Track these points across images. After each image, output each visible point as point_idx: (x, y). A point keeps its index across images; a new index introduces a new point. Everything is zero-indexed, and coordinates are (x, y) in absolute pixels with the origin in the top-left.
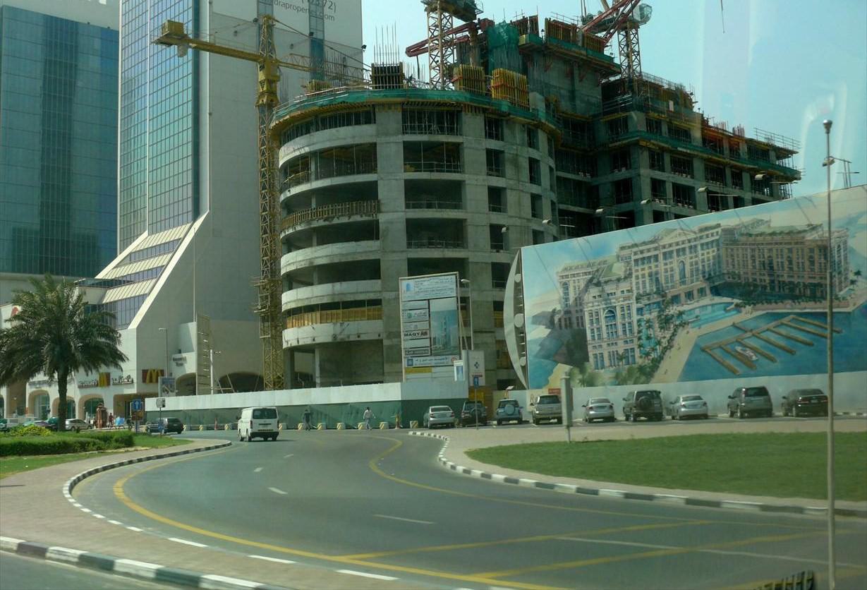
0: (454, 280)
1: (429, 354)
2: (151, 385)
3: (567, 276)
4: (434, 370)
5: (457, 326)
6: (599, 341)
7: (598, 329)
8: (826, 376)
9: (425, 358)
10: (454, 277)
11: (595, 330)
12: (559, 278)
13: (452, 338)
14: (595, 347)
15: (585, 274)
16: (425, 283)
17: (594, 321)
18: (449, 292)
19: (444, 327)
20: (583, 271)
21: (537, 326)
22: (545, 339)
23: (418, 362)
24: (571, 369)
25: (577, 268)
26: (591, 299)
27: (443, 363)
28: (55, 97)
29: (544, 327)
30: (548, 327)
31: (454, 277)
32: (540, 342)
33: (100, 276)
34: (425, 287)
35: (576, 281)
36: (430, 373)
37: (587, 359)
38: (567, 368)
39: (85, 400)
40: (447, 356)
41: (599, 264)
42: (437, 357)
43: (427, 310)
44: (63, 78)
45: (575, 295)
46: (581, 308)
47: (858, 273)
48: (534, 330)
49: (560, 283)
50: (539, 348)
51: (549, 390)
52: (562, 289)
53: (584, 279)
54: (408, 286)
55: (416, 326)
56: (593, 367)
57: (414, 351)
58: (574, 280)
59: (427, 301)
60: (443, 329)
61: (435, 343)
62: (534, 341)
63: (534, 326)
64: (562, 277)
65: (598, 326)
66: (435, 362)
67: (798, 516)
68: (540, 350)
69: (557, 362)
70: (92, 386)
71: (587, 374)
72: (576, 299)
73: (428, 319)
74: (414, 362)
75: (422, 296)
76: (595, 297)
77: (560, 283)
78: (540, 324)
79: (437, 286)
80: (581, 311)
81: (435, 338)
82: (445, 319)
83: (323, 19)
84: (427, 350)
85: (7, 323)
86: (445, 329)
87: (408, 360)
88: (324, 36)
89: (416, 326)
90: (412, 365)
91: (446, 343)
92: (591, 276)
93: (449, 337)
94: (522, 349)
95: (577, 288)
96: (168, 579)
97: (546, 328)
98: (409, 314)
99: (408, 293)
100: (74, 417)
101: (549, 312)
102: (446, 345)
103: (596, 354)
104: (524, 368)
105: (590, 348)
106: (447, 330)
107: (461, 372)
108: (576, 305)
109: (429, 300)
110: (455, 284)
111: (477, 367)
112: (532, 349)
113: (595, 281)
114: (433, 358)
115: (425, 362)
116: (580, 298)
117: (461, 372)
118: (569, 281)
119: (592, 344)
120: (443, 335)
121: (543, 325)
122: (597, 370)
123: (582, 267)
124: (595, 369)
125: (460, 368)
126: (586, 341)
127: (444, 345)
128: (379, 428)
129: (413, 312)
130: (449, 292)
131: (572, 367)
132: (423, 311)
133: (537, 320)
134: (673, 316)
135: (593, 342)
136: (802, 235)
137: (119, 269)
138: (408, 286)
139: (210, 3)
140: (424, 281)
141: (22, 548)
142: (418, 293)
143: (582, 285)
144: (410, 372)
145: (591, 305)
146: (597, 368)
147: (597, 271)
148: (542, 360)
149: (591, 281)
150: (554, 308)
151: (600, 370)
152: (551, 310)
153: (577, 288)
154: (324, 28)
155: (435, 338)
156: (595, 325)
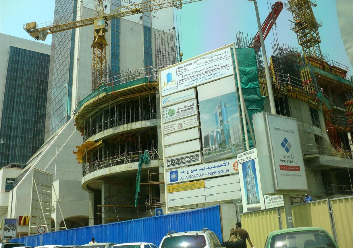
0: (229, 54)
2: (25, 227)
4: (207, 183)
5: (238, 114)
13: (231, 132)
18: (223, 71)
19: (220, 119)
27: (222, 172)
28: (32, 87)
34: (190, 72)
40: (227, 161)
42: (212, 165)
43: (195, 101)
54: (169, 76)
57: (178, 160)
61: (207, 144)
73: (196, 112)
74: (180, 175)
75: (187, 84)
79: (206, 67)
81: (207, 138)
82: (220, 107)
83: (151, 17)
84: (197, 155)
85: (54, 202)
86: (221, 121)
87: (171, 173)
88: (151, 26)
90: (177, 180)
91: (224, 141)
93: (228, 130)
96: (289, 168)
102: (223, 144)
106: (225, 122)
107: (250, 172)
109: (196, 88)
110: (230, 58)
111: (287, 150)
114: (206, 166)
115: (194, 173)
117: (250, 172)
125: (250, 165)
127: (220, 145)
129: (175, 108)
130: (223, 71)
132: (189, 103)
139: (81, 2)
142: (181, 82)
144: (177, 190)
154: (151, 22)
155: (207, 138)
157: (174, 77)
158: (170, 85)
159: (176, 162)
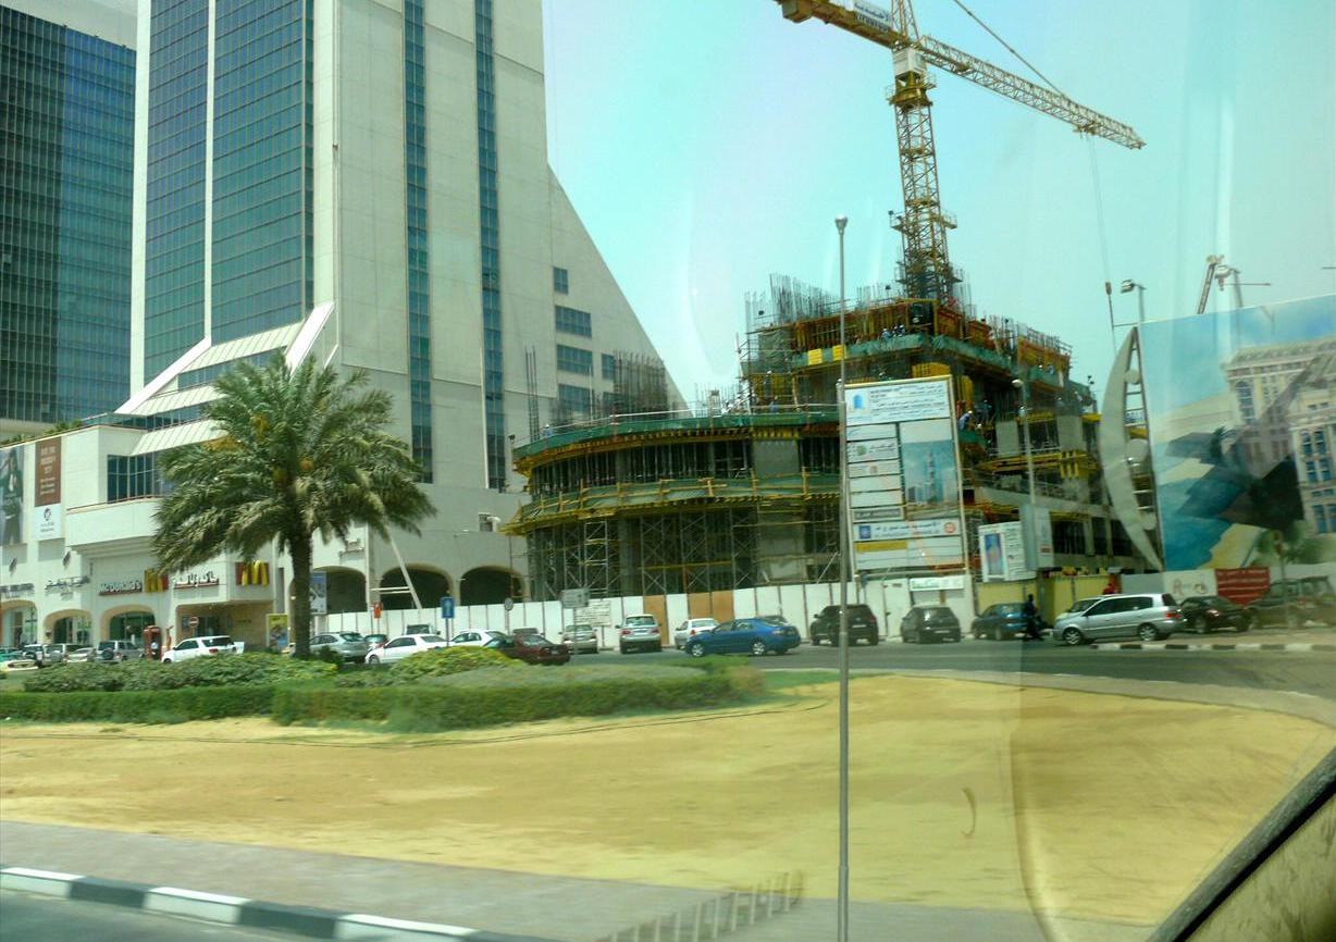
1: (901, 518)
3: (1245, 372)
4: (911, 544)
9: (894, 525)
10: (945, 382)
11: (1317, 464)
12: (1227, 374)
14: (1317, 494)
15: (1289, 366)
16: (890, 395)
17: (1314, 447)
19: (930, 470)
20: (1285, 362)
21: (1181, 459)
22: (1200, 482)
23: (881, 532)
24: (1263, 535)
26: (1305, 409)
27: (930, 532)
29: (1198, 460)
32: (1189, 486)
33: (125, 410)
36: (904, 551)
37: (1299, 513)
38: (1253, 532)
40: (937, 521)
41: (1320, 349)
44: (16, 103)
49: (1232, 382)
50: (1185, 498)
53: (1287, 376)
54: (857, 400)
57: (872, 512)
58: (1264, 378)
59: (893, 426)
61: (912, 499)
62: (1176, 487)
63: (1174, 460)
64: (1235, 372)
65: (1323, 457)
69: (1229, 522)
70: (130, 592)
71: (1301, 542)
72: (1269, 411)
75: (885, 416)
76: (1313, 407)
77: (1232, 382)
78: (1187, 456)
79: (913, 399)
80: (1284, 431)
89: (875, 468)
92: (1300, 370)
94: (1147, 500)
95: (1271, 391)
97: (1202, 462)
99: (859, 410)
100: (71, 641)
101: (1207, 435)
103: (1320, 506)
104: (1152, 535)
105: (1306, 496)
106: (937, 476)
108: (1271, 420)
109: (897, 424)
113: (1312, 378)
118: (1251, 380)
120: (929, 484)
121: (1196, 456)
122: (1322, 535)
123: (1280, 355)
124: (1320, 532)
126: (1296, 483)
128: (278, 653)
131: (1264, 530)
133: (1183, 447)
135: (1314, 485)
137: (160, 400)
138: (857, 400)
140: (889, 391)
141: (78, 891)
143: (1283, 385)
145: (1305, 420)
146: (1323, 529)
147: (1316, 360)
148: (1198, 519)
149: (1301, 379)
150: (1220, 427)
152: (1213, 431)
153: (1271, 391)
157: (865, 402)
158: (858, 412)
159: (869, 514)
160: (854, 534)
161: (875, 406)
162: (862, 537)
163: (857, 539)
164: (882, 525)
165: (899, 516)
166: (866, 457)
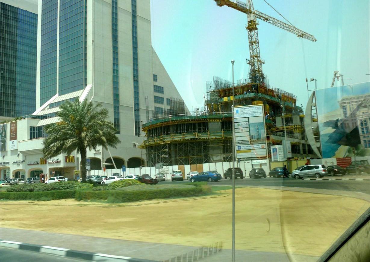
0: (262, 108)
3: (345, 103)
4: (252, 151)
6: (367, 134)
7: (366, 128)
8: (196, 165)
12: (340, 104)
14: (364, 137)
16: (246, 110)
19: (257, 130)
21: (327, 127)
22: (332, 134)
23: (244, 148)
24: (350, 148)
25: (351, 99)
26: (361, 114)
27: (257, 148)
29: (331, 128)
30: (333, 128)
31: (261, 106)
32: (329, 135)
35: (351, 105)
39: (31, 170)
40: (259, 145)
41: (365, 97)
45: (351, 112)
46: (355, 118)
47: (301, 105)
48: (325, 129)
49: (341, 106)
50: (328, 138)
51: (337, 158)
52: (342, 109)
53: (356, 104)
54: (237, 111)
55: (242, 130)
56: (364, 147)
57: (241, 142)
59: (247, 118)
60: (257, 132)
62: (325, 135)
63: (325, 128)
65: (366, 127)
66: (253, 147)
67: (34, 254)
68: (329, 139)
69: (340, 145)
70: (36, 164)
71: (360, 150)
72: (351, 114)
75: (245, 116)
78: (328, 127)
80: (355, 120)
84: (249, 141)
90: (241, 149)
97: (333, 128)
98: (238, 124)
99: (238, 114)
104: (319, 148)
105: (361, 138)
106: (259, 132)
109: (248, 118)
112: (324, 139)
113: (363, 105)
116: (354, 114)
118: (346, 105)
119: (363, 135)
120: (257, 134)
122: (366, 148)
131: (350, 147)
133: (327, 124)
134: (103, 132)
136: (225, 85)
138: (237, 111)
140: (246, 108)
146: (366, 147)
147: (364, 100)
149: (360, 105)
150: (337, 118)
151: (368, 148)
152: (335, 120)
156: (364, 126)
157: (239, 112)
158: (237, 114)
159: (240, 143)
160: (236, 148)
161: (242, 113)
162: (238, 149)
163: (237, 149)
164: (244, 146)
165: (249, 143)
166: (240, 127)
